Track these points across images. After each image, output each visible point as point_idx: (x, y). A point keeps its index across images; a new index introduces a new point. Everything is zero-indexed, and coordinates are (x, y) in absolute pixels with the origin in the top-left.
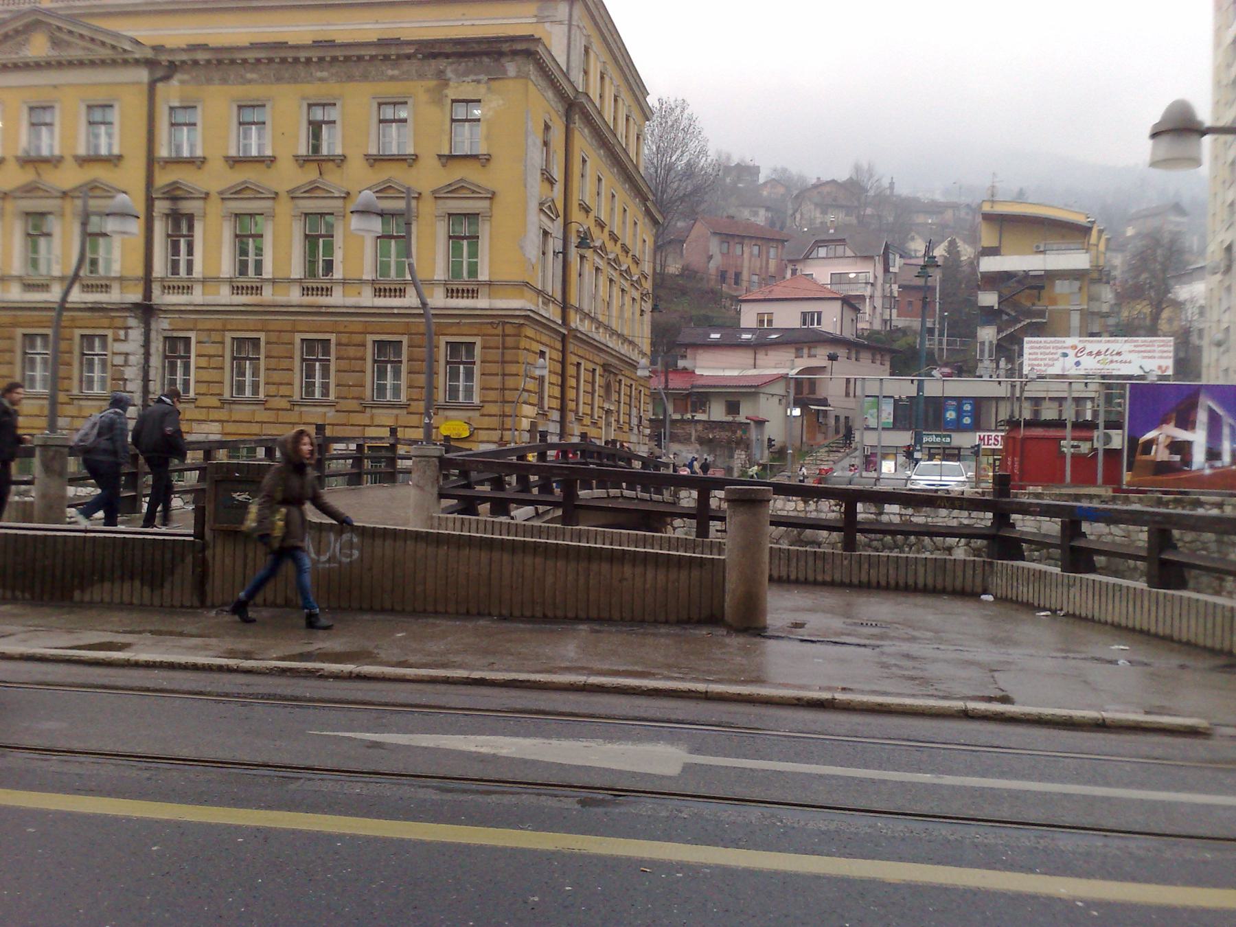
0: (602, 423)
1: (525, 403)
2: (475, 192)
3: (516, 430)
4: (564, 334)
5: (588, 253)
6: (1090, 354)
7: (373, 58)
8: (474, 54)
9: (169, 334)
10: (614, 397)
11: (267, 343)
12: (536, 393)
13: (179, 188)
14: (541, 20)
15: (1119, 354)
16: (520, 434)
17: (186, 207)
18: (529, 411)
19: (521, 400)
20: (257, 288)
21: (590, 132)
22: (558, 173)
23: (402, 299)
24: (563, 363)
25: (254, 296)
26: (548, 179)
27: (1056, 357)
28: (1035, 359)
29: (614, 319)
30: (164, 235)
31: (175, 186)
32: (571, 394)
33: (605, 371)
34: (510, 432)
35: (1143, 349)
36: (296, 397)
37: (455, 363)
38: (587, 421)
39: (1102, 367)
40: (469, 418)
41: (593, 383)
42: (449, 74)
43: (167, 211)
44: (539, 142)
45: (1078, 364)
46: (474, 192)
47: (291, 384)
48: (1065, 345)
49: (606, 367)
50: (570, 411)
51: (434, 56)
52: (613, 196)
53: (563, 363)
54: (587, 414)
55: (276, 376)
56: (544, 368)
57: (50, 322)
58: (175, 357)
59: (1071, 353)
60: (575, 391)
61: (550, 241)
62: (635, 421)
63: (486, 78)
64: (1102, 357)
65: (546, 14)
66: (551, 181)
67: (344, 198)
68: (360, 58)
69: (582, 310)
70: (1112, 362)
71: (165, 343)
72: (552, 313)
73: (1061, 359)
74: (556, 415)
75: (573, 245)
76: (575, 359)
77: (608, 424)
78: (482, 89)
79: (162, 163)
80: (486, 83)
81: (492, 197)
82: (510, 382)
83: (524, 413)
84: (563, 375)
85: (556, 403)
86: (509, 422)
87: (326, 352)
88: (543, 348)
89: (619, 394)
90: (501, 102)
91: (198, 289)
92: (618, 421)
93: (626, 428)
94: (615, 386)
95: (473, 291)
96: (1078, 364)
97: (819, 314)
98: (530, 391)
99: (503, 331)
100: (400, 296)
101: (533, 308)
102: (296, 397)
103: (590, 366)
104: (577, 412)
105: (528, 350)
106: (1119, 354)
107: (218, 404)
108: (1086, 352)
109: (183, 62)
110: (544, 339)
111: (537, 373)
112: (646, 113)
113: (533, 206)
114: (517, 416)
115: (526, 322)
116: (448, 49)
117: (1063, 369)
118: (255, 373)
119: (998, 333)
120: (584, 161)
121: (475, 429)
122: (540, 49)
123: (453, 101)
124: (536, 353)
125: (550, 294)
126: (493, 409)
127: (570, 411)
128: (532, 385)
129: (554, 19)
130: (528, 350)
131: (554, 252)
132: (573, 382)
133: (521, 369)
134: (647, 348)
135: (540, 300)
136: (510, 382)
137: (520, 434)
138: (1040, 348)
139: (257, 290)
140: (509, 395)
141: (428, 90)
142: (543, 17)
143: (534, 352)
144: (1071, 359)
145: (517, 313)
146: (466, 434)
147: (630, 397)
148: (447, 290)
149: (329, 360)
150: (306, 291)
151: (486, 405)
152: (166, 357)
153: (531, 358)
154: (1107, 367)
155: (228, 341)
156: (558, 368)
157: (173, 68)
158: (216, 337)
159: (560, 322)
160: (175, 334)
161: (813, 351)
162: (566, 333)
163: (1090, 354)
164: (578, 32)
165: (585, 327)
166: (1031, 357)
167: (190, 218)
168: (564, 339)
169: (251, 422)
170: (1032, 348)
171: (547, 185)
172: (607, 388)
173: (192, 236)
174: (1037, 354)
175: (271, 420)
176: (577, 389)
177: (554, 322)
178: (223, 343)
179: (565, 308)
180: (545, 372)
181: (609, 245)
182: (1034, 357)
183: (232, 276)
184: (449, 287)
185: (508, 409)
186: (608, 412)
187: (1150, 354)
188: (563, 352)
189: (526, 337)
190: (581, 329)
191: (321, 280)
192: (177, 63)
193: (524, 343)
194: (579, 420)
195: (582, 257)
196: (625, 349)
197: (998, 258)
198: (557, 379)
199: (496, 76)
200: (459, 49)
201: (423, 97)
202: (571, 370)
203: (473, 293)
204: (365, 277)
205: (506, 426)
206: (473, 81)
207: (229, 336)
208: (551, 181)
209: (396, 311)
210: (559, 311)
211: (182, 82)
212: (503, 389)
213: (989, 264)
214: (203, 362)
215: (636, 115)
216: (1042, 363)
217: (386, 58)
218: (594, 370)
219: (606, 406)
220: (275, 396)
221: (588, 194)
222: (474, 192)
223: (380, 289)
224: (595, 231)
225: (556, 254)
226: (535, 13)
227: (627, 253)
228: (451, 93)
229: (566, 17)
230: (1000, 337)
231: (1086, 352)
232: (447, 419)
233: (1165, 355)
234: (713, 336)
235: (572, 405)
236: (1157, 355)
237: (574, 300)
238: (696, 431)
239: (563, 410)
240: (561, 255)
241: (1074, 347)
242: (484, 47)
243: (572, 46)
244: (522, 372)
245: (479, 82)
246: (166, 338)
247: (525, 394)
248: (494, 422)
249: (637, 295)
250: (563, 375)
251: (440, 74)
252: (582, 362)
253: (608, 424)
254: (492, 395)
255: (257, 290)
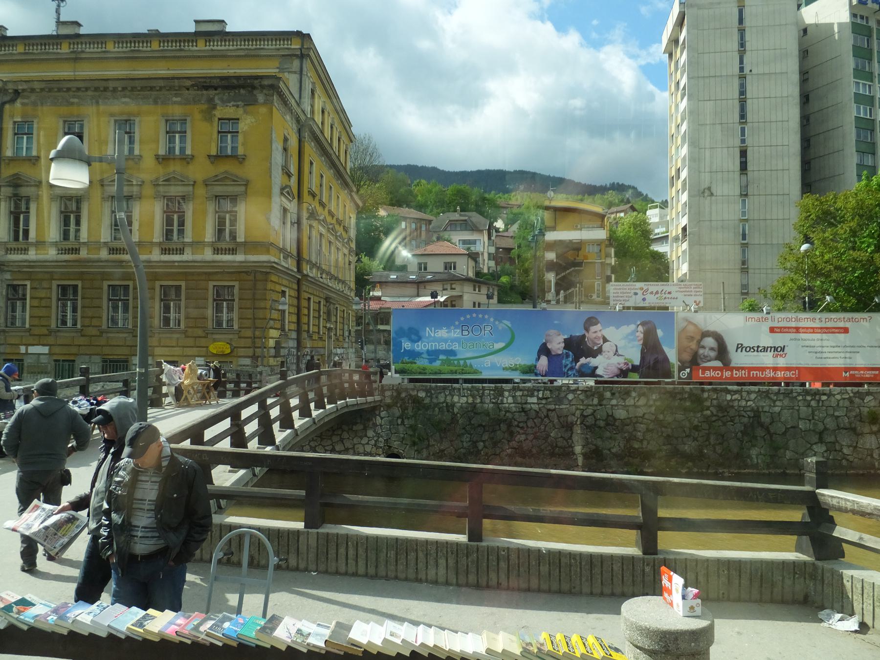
0: (326, 338)
1: (271, 328)
2: (235, 180)
3: (265, 348)
4: (299, 279)
5: (315, 224)
6: (652, 293)
7: (161, 88)
8: (234, 87)
9: (10, 282)
10: (333, 319)
11: (83, 288)
12: (279, 320)
13: (20, 179)
14: (282, 70)
15: (669, 293)
16: (268, 351)
17: (24, 191)
18: (274, 333)
19: (269, 326)
20: (76, 249)
21: (315, 145)
22: (293, 169)
23: (234, 256)
24: (298, 298)
25: (178, 256)
26: (286, 173)
27: (630, 295)
28: (618, 297)
29: (332, 267)
30: (7, 212)
31: (17, 176)
32: (304, 319)
33: (327, 302)
34: (260, 350)
35: (684, 290)
36: (104, 327)
37: (220, 300)
38: (315, 337)
39: (659, 301)
40: (231, 339)
41: (319, 311)
42: (217, 101)
43: (10, 195)
44: (280, 147)
45: (644, 299)
46: (234, 181)
47: (100, 318)
48: (636, 287)
49: (327, 299)
50: (304, 331)
51: (206, 88)
52: (331, 187)
53: (298, 298)
54: (315, 332)
55: (90, 313)
56: (286, 305)
57: (4, 271)
58: (66, 300)
59: (640, 292)
60: (307, 317)
61: (289, 215)
62: (346, 334)
63: (243, 104)
64: (659, 295)
65: (286, 66)
66: (289, 175)
67: (141, 185)
68: (152, 88)
69: (311, 262)
70: (665, 298)
71: (7, 289)
72: (291, 264)
73: (634, 296)
74: (294, 335)
75: (304, 218)
76: (306, 296)
77: (330, 337)
78: (241, 111)
79: (7, 161)
80: (243, 107)
81: (247, 183)
82: (260, 313)
83: (271, 335)
84: (299, 308)
85: (293, 327)
86: (258, 343)
87: (126, 293)
88: (283, 289)
89: (336, 316)
90: (253, 120)
91: (188, 250)
92: (336, 335)
93: (341, 338)
94: (333, 312)
95: (233, 249)
96: (644, 299)
97: (455, 263)
98: (276, 320)
99: (255, 277)
100: (180, 254)
101: (276, 260)
102: (104, 327)
103: (317, 300)
104: (308, 331)
105: (273, 291)
106: (669, 293)
107: (46, 332)
108: (649, 292)
109: (24, 90)
110: (285, 282)
111: (281, 307)
112: (351, 138)
113: (276, 190)
114: (265, 338)
115: (272, 271)
116: (215, 82)
117: (635, 303)
118: (74, 310)
119: (557, 275)
120: (311, 163)
121: (235, 347)
122: (281, 85)
123: (219, 119)
124: (279, 293)
125: (289, 251)
126: (248, 333)
127: (304, 331)
128: (275, 315)
129: (291, 70)
130: (273, 291)
131: (291, 222)
132: (305, 311)
133: (268, 304)
134: (353, 285)
135: (282, 255)
136: (260, 313)
137: (268, 351)
138: (620, 289)
139: (76, 251)
140: (259, 323)
141: (202, 111)
142: (283, 69)
143: (277, 292)
144: (640, 296)
145: (265, 264)
146: (228, 351)
147: (343, 318)
148: (214, 249)
149: (128, 300)
150: (113, 250)
151: (243, 330)
152: (8, 299)
153: (275, 296)
154: (662, 301)
155: (54, 287)
156: (295, 302)
157: (17, 93)
158: (45, 284)
159: (296, 270)
160: (15, 283)
161: (454, 286)
162: (300, 277)
163: (652, 293)
164: (307, 79)
165: (314, 273)
166: (615, 295)
167: (28, 200)
168: (299, 282)
169: (71, 345)
170: (615, 289)
171: (287, 177)
172: (328, 313)
173: (29, 212)
174: (618, 293)
175: (86, 344)
176: (309, 316)
177: (292, 270)
178: (50, 288)
179: (299, 260)
180: (286, 307)
181: (329, 219)
182: (616, 295)
183: (58, 240)
184: (216, 246)
185: (257, 333)
186: (330, 329)
187: (689, 293)
188: (298, 291)
189: (271, 281)
190: (311, 275)
191: (71, 243)
192: (20, 91)
193: (270, 286)
194: (310, 337)
195: (311, 226)
196: (340, 287)
197: (555, 232)
198: (294, 310)
199: (251, 102)
200: (224, 83)
201: (198, 116)
202: (304, 303)
203: (233, 251)
204: (155, 240)
205: (257, 345)
206: (233, 106)
207: (55, 284)
208: (289, 175)
209: (176, 264)
210: (295, 263)
211: (23, 104)
212: (255, 319)
213: (550, 236)
214: (36, 303)
215: (344, 138)
216: (622, 299)
217: (171, 88)
218: (320, 302)
219: (328, 325)
220: (89, 326)
221: (314, 184)
222: (234, 181)
223: (166, 249)
224: (319, 209)
225: (292, 224)
226: (278, 65)
227: (340, 225)
228: (219, 113)
229: (298, 69)
230: (558, 277)
231: (649, 292)
232: (215, 340)
233: (698, 293)
234: (392, 277)
235: (305, 327)
236: (693, 293)
237: (305, 255)
238: (384, 337)
239: (299, 331)
240: (296, 225)
241: (641, 289)
242: (241, 82)
243: (303, 88)
244: (268, 307)
245: (238, 106)
246: (8, 285)
247: (272, 322)
248: (248, 342)
249: (346, 251)
250: (299, 308)
251: (210, 100)
252: (312, 297)
253: (330, 337)
254: (248, 323)
255: (76, 251)
